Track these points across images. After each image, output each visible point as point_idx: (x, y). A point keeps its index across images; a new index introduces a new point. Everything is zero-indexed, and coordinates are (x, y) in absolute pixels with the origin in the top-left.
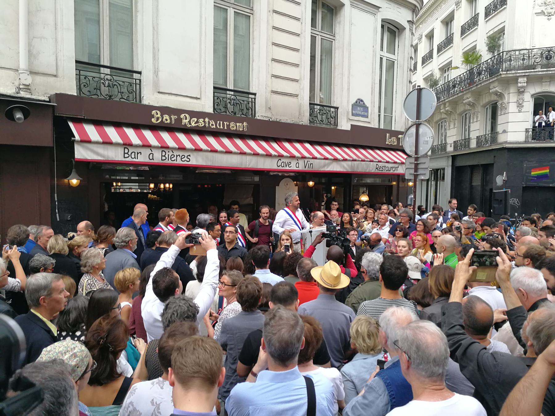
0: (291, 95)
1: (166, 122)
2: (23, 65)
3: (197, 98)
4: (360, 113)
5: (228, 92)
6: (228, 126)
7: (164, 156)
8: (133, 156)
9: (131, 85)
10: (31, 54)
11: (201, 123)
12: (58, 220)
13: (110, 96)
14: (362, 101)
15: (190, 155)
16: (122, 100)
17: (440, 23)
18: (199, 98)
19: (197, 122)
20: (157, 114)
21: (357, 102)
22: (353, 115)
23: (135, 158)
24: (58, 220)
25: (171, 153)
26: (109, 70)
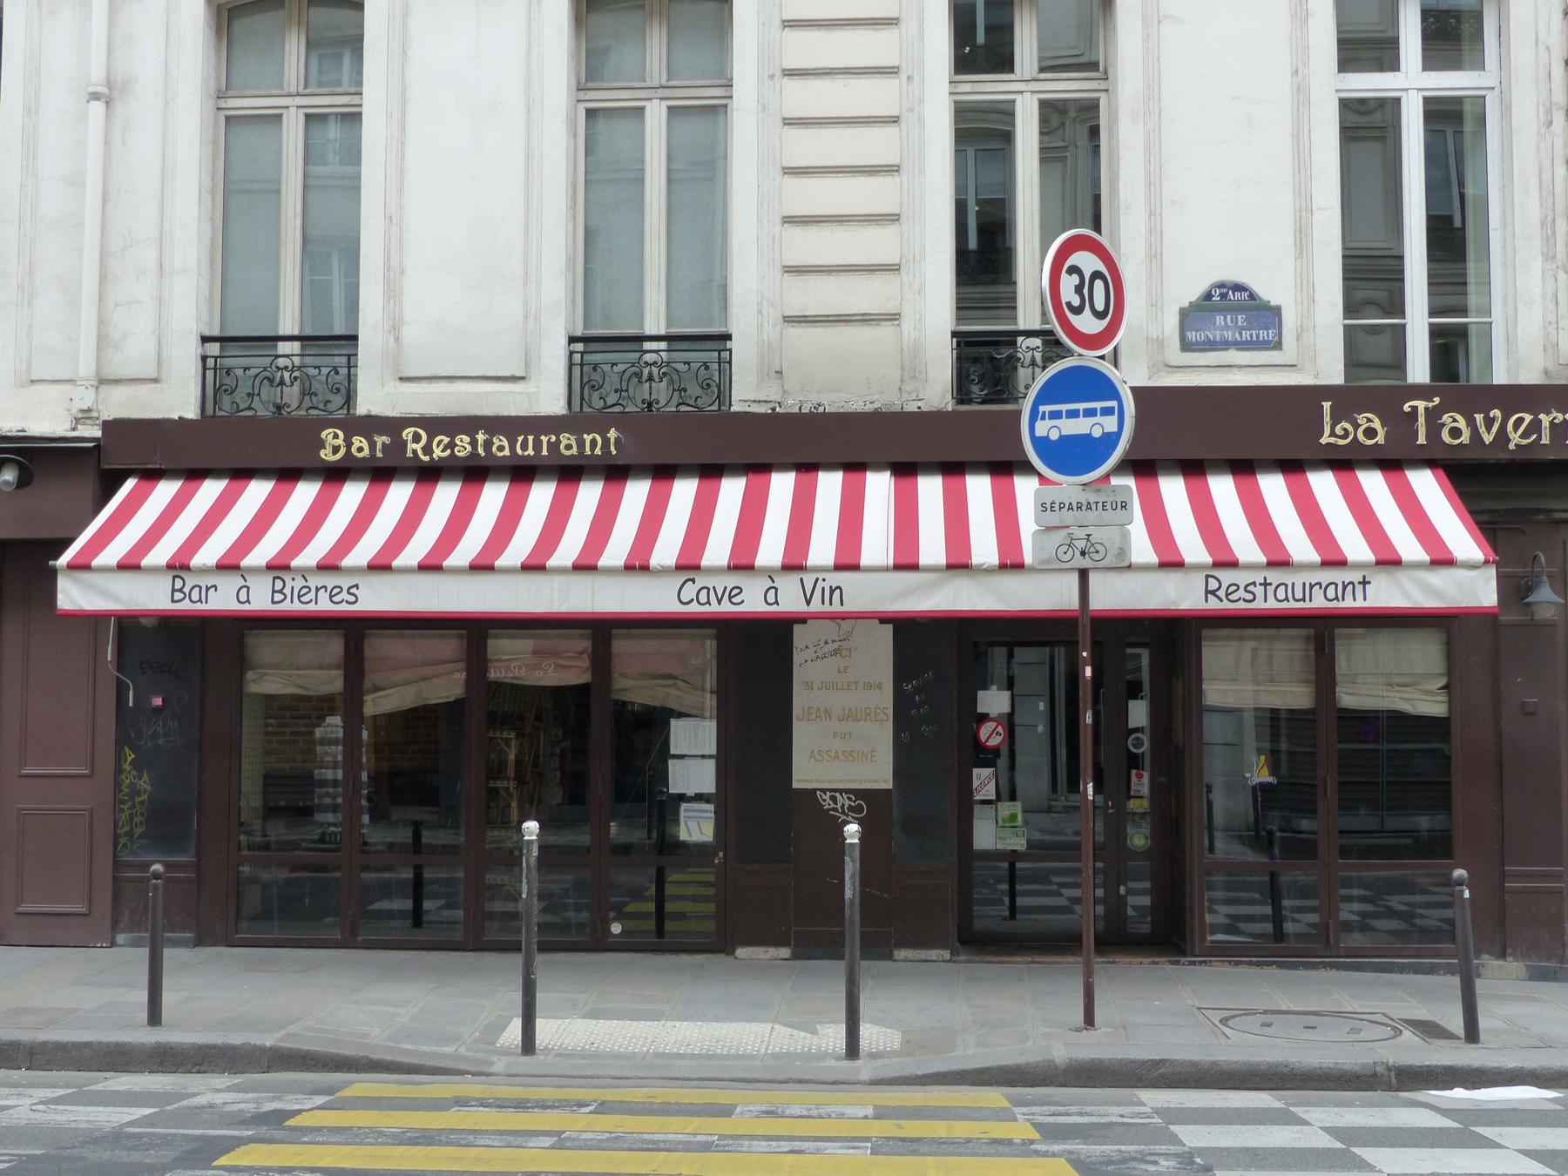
0: (866, 319)
2: (86, 369)
4: (1229, 335)
5: (647, 345)
6: (554, 447)
7: (281, 592)
8: (195, 596)
9: (707, 368)
10: (102, 341)
13: (650, 405)
14: (1238, 288)
15: (357, 586)
16: (683, 408)
18: (523, 378)
20: (336, 436)
21: (1208, 296)
22: (1186, 346)
23: (1287, 599)
25: (299, 582)
26: (217, 345)
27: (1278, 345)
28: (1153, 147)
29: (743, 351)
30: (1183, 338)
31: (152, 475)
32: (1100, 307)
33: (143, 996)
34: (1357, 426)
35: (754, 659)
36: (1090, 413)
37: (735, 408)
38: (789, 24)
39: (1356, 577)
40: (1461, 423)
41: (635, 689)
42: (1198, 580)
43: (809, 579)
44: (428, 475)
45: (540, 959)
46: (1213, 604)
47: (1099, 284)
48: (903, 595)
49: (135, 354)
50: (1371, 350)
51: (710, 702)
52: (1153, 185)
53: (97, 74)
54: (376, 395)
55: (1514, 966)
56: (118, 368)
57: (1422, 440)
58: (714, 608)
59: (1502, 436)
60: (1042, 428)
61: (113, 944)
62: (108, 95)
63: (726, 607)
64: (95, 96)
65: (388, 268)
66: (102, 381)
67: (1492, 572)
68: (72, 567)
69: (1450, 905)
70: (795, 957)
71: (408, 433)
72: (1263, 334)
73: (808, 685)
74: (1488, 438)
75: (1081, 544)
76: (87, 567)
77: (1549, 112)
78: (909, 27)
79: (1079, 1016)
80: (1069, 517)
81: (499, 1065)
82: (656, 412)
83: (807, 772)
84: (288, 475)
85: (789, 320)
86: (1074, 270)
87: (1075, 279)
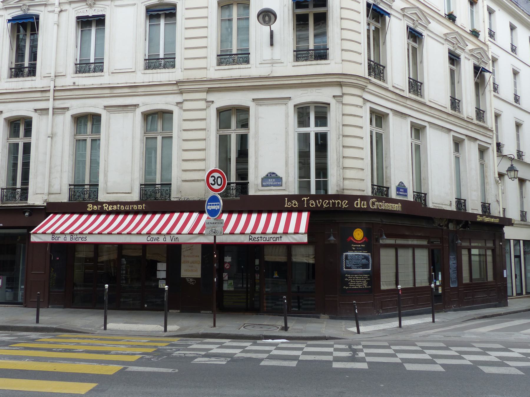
1: (355, 206)
2: (46, 191)
3: (129, 193)
4: (271, 183)
10: (50, 186)
11: (115, 207)
12: (440, 273)
14: (274, 173)
17: (140, 114)
19: (113, 207)
21: (267, 175)
22: (263, 186)
24: (440, 273)
27: (281, 185)
28: (256, 144)
29: (174, 188)
30: (262, 184)
31: (56, 214)
32: (219, 183)
33: (35, 317)
34: (292, 203)
35: (173, 252)
36: (216, 205)
37: (172, 199)
38: (184, 120)
39: (279, 236)
40: (314, 203)
41: (149, 256)
42: (248, 236)
43: (172, 236)
44: (109, 213)
45: (108, 311)
46: (251, 241)
47: (219, 179)
48: (190, 239)
49: (56, 188)
50: (304, 185)
51: (165, 259)
52: (256, 152)
53: (49, 132)
54: (102, 197)
55: (327, 316)
56: (52, 192)
57: (306, 206)
58: (154, 242)
59: (322, 205)
60: (209, 207)
61: (48, 307)
62: (52, 137)
63: (156, 242)
64: (49, 137)
65: (105, 170)
66: (49, 194)
67: (306, 235)
68: (33, 233)
69: (282, 305)
70: (181, 312)
71: (104, 205)
72: (278, 183)
73: (184, 256)
74: (319, 206)
75: (214, 231)
76: (36, 233)
77: (339, 136)
78: (208, 121)
79: (213, 325)
80: (212, 225)
81: (98, 332)
82: (156, 200)
83: (184, 274)
84: (81, 214)
85: (183, 181)
86: (212, 177)
87: (213, 178)
